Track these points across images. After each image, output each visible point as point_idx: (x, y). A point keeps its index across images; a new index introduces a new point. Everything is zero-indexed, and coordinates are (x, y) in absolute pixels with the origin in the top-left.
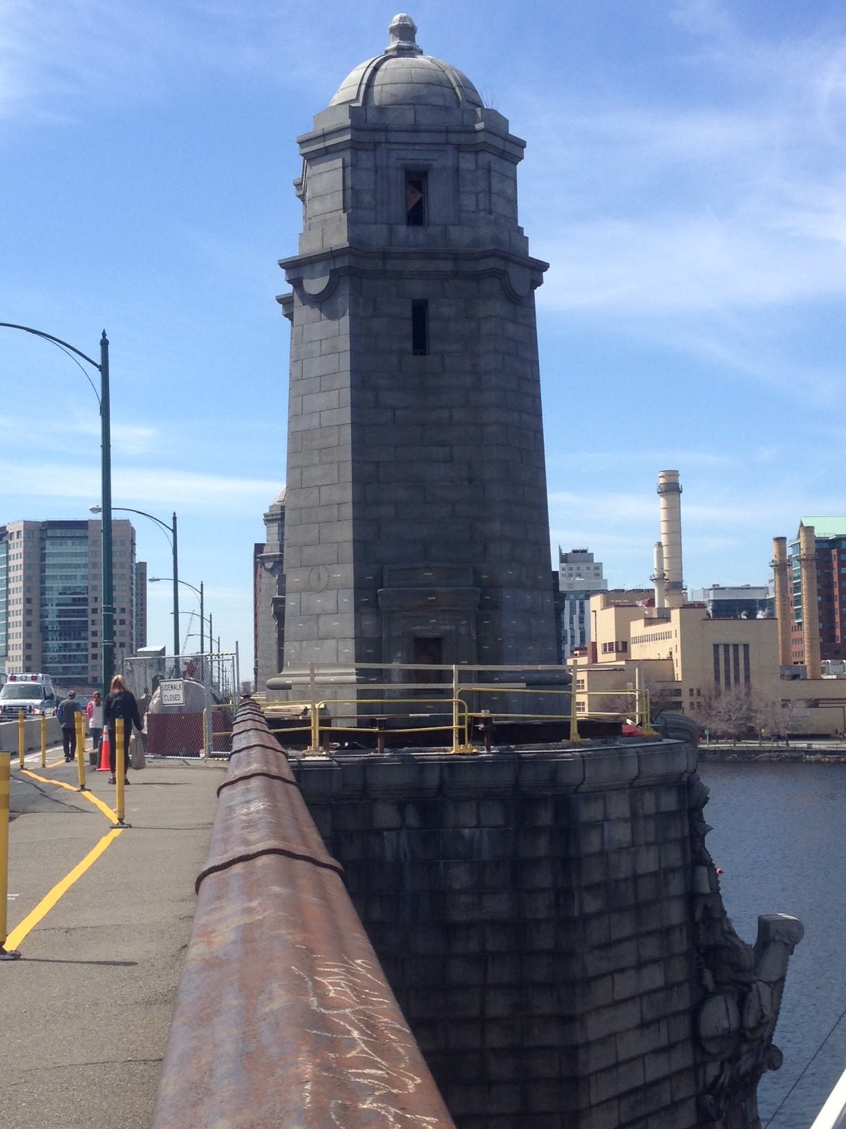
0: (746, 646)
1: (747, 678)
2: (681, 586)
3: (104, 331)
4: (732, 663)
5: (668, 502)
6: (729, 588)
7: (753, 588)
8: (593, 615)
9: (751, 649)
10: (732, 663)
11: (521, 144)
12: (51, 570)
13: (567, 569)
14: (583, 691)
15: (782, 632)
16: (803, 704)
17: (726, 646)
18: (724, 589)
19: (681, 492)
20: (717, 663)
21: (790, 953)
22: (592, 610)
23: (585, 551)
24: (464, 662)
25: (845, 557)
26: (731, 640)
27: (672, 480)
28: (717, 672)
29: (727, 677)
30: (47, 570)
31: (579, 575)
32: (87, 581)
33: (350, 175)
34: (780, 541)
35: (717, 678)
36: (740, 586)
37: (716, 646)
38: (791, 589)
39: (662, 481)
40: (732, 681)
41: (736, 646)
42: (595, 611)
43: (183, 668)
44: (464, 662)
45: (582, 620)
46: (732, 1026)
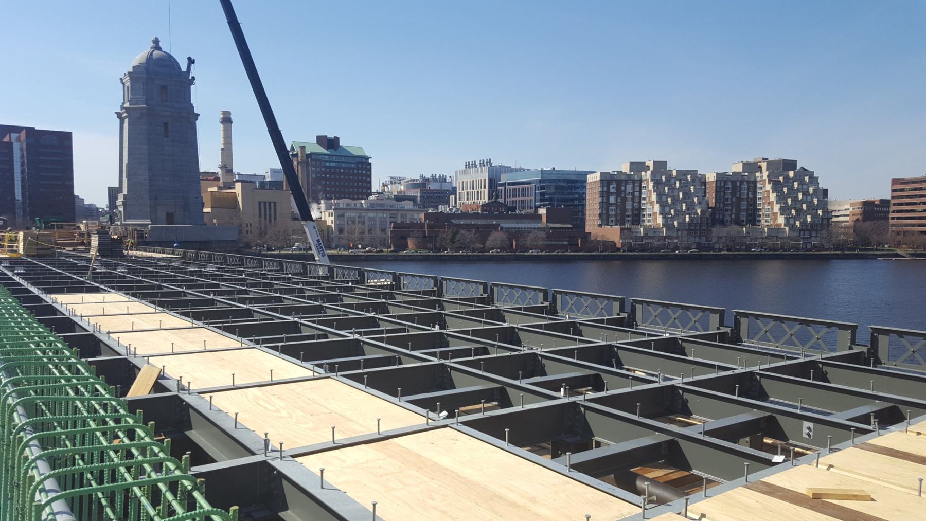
0: (275, 203)
1: (275, 219)
3: (875, 501)
4: (268, 211)
5: (225, 128)
7: (257, 175)
9: (277, 204)
10: (268, 211)
17: (265, 203)
19: (232, 123)
21: (623, 237)
25: (925, 247)
27: (228, 116)
29: (270, 219)
33: (813, 331)
36: (250, 174)
37: (260, 203)
38: (501, 198)
39: (222, 116)
40: (273, 220)
43: (57, 391)
46: (36, 444)
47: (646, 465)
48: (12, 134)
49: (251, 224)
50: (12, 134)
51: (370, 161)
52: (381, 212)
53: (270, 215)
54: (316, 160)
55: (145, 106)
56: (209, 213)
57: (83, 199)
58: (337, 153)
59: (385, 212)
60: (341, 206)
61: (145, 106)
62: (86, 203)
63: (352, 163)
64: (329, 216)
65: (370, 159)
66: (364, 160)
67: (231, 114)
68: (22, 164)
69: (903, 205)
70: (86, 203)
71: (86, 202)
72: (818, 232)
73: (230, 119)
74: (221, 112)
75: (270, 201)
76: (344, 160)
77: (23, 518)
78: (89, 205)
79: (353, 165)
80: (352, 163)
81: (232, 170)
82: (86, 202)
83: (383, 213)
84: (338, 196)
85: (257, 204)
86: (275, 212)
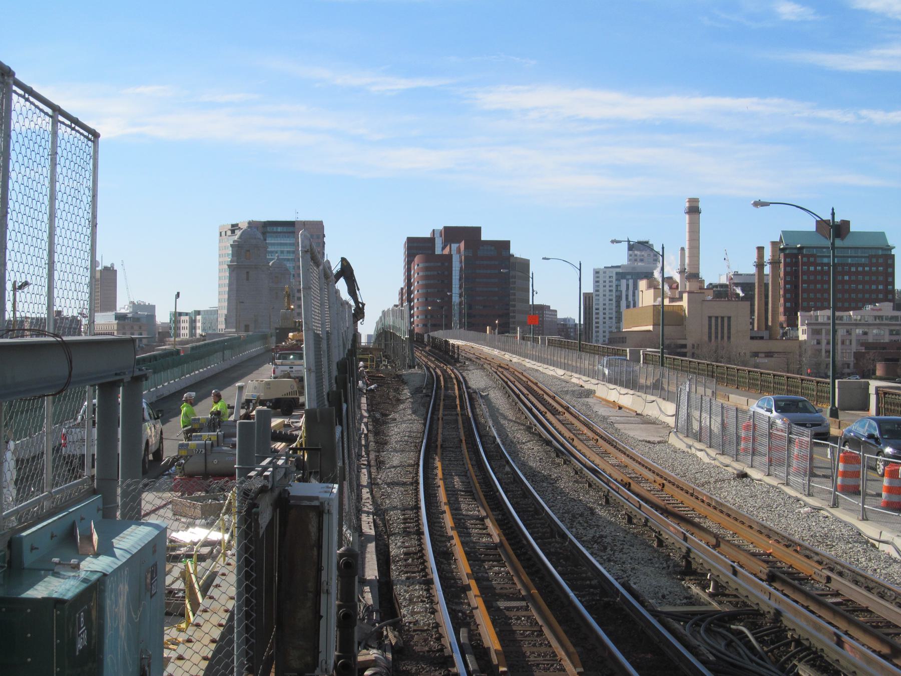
0: (729, 318)
1: (729, 338)
2: (698, 276)
6: (745, 274)
8: (641, 293)
9: (732, 319)
11: (556, 311)
12: (270, 239)
13: (633, 256)
15: (72, 336)
16: (763, 355)
17: (717, 318)
18: (741, 275)
20: (710, 328)
22: (640, 290)
23: (647, 242)
24: (313, 529)
26: (725, 313)
27: (694, 204)
28: (710, 333)
30: (267, 239)
31: (642, 260)
32: (294, 247)
34: (760, 250)
35: (710, 337)
37: (710, 318)
41: (723, 318)
42: (642, 291)
44: (313, 529)
45: (634, 295)
47: (167, 351)
48: (452, 245)
50: (452, 245)
51: (893, 252)
52: (876, 327)
53: (722, 333)
54: (808, 256)
55: (121, 388)
56: (649, 331)
57: (556, 311)
58: (847, 242)
59: (882, 327)
60: (820, 320)
61: (121, 388)
62: (559, 317)
63: (862, 257)
64: (803, 334)
65: (892, 250)
66: (886, 253)
67: (699, 202)
68: (460, 279)
70: (559, 317)
71: (560, 315)
73: (698, 208)
74: (687, 200)
75: (722, 315)
76: (850, 253)
78: (565, 320)
79: (863, 260)
80: (862, 257)
81: (698, 274)
82: (560, 315)
83: (879, 328)
84: (819, 304)
85: (707, 318)
86: (729, 329)
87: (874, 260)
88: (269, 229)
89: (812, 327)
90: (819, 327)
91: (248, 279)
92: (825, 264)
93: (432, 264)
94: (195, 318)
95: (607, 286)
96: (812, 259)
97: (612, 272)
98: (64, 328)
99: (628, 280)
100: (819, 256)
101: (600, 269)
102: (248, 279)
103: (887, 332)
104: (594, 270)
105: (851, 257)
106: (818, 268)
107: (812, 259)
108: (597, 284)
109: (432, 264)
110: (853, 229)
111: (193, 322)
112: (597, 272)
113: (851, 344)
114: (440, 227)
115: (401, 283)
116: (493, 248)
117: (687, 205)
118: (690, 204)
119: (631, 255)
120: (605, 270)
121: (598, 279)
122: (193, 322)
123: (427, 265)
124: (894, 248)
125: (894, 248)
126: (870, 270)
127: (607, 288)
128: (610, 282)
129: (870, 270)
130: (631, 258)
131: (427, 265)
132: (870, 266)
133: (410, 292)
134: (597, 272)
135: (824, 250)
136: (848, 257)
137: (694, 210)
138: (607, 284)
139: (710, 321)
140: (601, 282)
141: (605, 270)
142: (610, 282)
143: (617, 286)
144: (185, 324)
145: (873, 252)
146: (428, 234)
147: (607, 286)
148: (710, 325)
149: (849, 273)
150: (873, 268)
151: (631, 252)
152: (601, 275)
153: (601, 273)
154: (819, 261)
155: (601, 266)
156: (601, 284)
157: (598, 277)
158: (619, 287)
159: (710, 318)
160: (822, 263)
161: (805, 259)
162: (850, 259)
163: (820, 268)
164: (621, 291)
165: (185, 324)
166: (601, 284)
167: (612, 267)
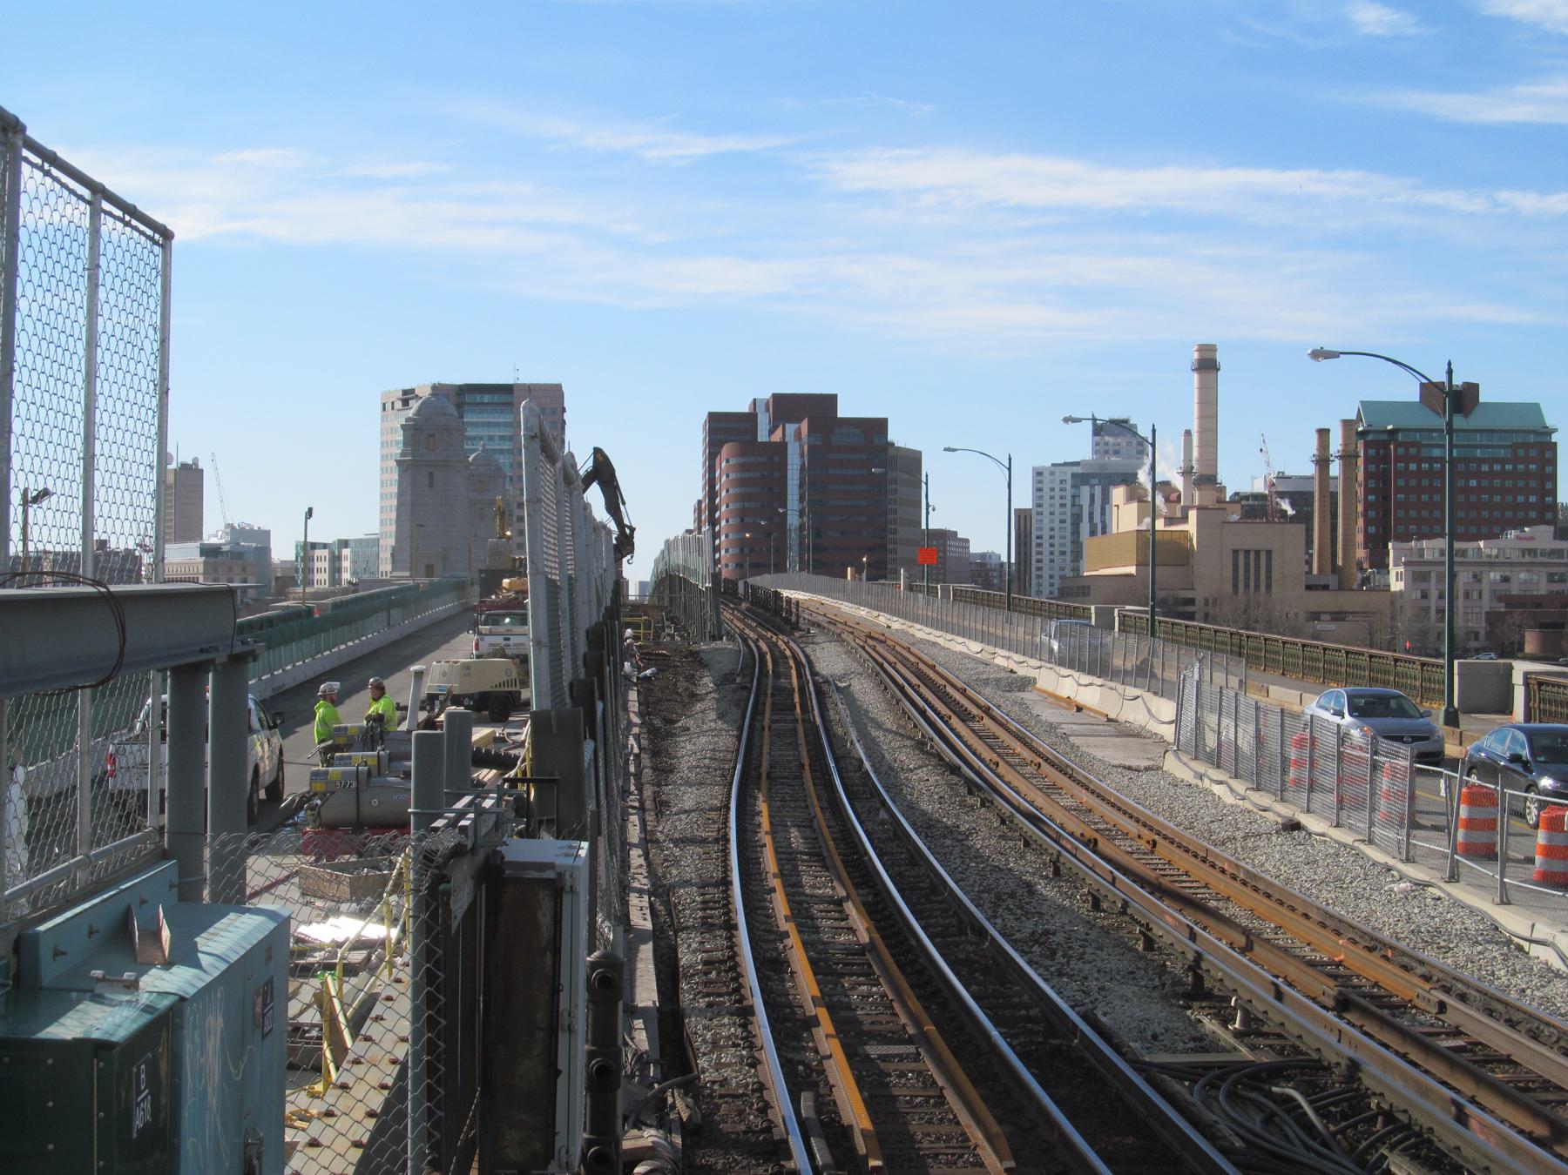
0: (1269, 553)
1: (1269, 587)
2: (1215, 480)
6: (1296, 477)
8: (1115, 509)
9: (1274, 555)
12: (469, 415)
13: (1102, 444)
14: (1561, 561)
16: (1328, 617)
17: (1247, 552)
18: (1290, 478)
20: (1236, 570)
22: (1114, 504)
23: (1126, 421)
24: (545, 919)
26: (1262, 545)
27: (1208, 355)
28: (1235, 579)
30: (465, 415)
31: (1117, 453)
32: (512, 430)
34: (1323, 434)
35: (1235, 586)
37: (1236, 552)
41: (1257, 553)
42: (1118, 506)
44: (545, 919)
45: (1103, 513)
48: (787, 426)
49: (469, 675)
50: (787, 426)
51: (1555, 437)
52: (1524, 568)
53: (1257, 578)
54: (1407, 445)
57: (967, 541)
58: (1473, 421)
59: (1535, 569)
60: (1427, 556)
62: (972, 550)
63: (1500, 447)
64: (1397, 580)
65: (1553, 435)
66: (1542, 439)
67: (1216, 350)
68: (801, 485)
69: (1332, 519)
70: (972, 550)
71: (975, 548)
72: (466, 408)
73: (1215, 361)
74: (1196, 347)
75: (1257, 548)
76: (1479, 439)
77: (1565, 687)
78: (983, 556)
79: (1502, 451)
80: (1500, 447)
81: (1215, 477)
82: (975, 548)
83: (1529, 571)
84: (1425, 529)
85: (1231, 554)
86: (1269, 572)
87: (1521, 453)
88: (468, 398)
89: (1413, 568)
90: (1425, 569)
91: (431, 485)
92: (1436, 458)
93: (752, 459)
94: (340, 552)
95: (1057, 498)
96: (1413, 451)
97: (1065, 473)
98: (112, 570)
99: (1092, 486)
100: (1425, 446)
101: (1045, 468)
102: (431, 485)
103: (1544, 578)
104: (1034, 469)
105: (1480, 446)
106: (1423, 465)
107: (1413, 451)
108: (1040, 494)
109: (752, 459)
110: (1484, 397)
111: (336, 560)
112: (1038, 473)
113: (1480, 598)
114: (765, 394)
115: (698, 492)
116: (858, 431)
117: (1196, 356)
118: (1200, 355)
119: (1097, 444)
120: (1053, 469)
121: (1040, 486)
122: (336, 560)
123: (743, 460)
124: (1556, 430)
125: (1556, 430)
126: (1515, 469)
127: (1057, 501)
128: (1061, 490)
129: (1515, 469)
130: (1098, 448)
131: (743, 460)
132: (1515, 463)
133: (713, 508)
134: (1038, 473)
135: (1435, 435)
136: (1476, 447)
137: (1207, 364)
138: (1057, 494)
139: (1235, 558)
140: (1046, 490)
141: (1053, 469)
142: (1061, 490)
143: (1073, 497)
144: (321, 563)
145: (1519, 439)
146: (744, 408)
147: (1057, 498)
148: (1235, 565)
149: (1478, 475)
150: (1519, 466)
151: (1097, 438)
152: (1046, 477)
153: (1046, 474)
154: (1425, 453)
155: (1046, 462)
156: (1046, 493)
157: (1040, 482)
158: (1077, 499)
159: (1236, 552)
160: (1431, 458)
161: (1401, 451)
162: (1479, 451)
163: (1427, 466)
164: (1081, 506)
165: (321, 563)
166: (1046, 493)
167: (1066, 464)
